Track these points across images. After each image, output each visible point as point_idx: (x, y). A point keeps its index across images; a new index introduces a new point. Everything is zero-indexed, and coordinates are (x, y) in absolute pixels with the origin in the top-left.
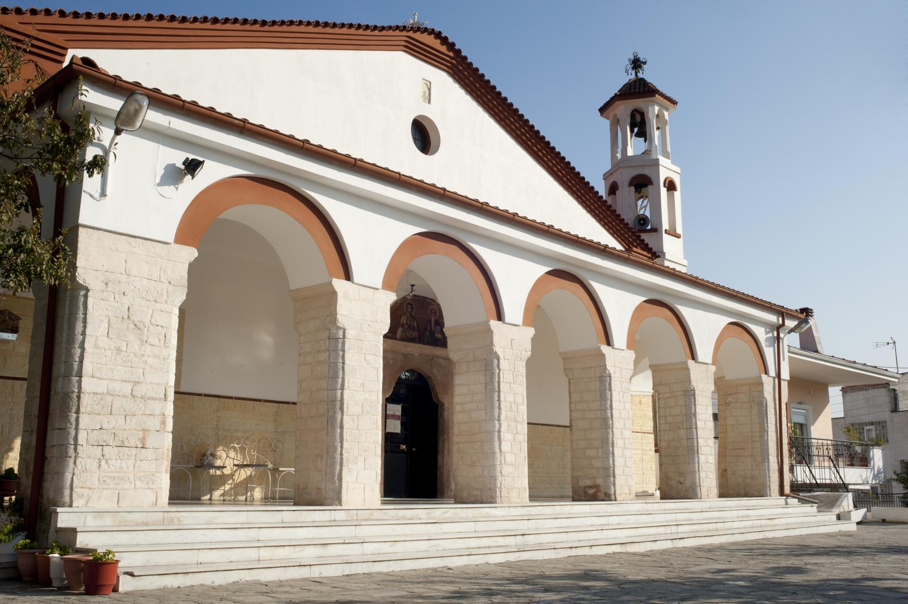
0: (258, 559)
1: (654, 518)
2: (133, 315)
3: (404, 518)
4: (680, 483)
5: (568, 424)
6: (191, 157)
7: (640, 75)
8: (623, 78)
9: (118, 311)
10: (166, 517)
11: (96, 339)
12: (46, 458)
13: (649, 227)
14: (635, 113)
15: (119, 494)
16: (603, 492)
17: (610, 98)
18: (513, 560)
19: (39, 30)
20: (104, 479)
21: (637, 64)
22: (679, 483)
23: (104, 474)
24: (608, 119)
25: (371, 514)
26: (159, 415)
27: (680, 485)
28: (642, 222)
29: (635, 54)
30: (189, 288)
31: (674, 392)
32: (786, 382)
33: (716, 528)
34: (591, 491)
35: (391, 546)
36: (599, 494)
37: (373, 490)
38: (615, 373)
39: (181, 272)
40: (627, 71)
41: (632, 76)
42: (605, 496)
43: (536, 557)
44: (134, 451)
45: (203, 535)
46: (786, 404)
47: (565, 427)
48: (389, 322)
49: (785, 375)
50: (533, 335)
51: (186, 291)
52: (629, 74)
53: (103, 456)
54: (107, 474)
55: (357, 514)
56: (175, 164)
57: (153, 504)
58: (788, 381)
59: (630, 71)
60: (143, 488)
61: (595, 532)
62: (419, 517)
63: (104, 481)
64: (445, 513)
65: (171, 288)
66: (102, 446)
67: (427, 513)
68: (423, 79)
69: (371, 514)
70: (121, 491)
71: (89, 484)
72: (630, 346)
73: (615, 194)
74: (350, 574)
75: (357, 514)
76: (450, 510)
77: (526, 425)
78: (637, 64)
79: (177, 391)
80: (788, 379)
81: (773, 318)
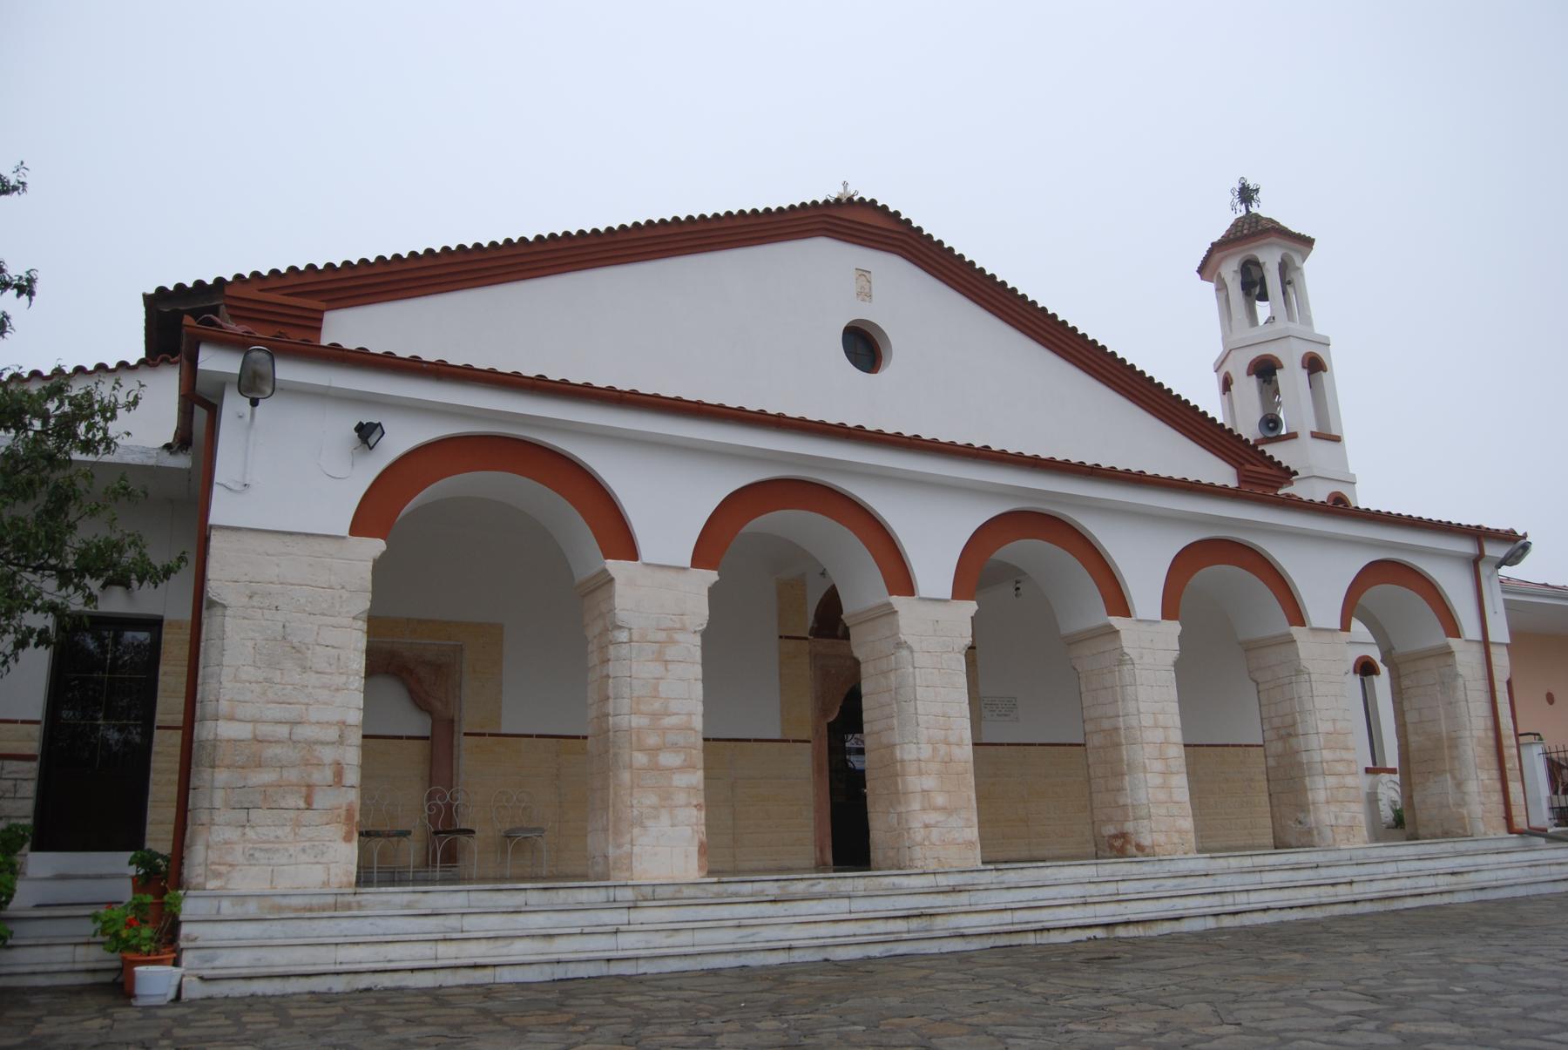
0: (434, 957)
1: (1215, 880)
2: (289, 635)
3: (736, 895)
4: (1300, 823)
5: (1262, 743)
6: (366, 419)
7: (1253, 209)
8: (1222, 217)
9: (269, 632)
10: (338, 900)
11: (237, 670)
12: (1504, 818)
13: (1284, 432)
14: (1249, 266)
15: (272, 871)
16: (1134, 843)
17: (1208, 251)
18: (878, 955)
19: (285, 295)
20: (251, 852)
21: (1246, 194)
22: (1297, 823)
23: (251, 845)
24: (1212, 281)
25: (679, 891)
26: (330, 765)
27: (1299, 826)
28: (1271, 425)
29: (1243, 181)
30: (373, 592)
31: (1279, 678)
32: (1504, 650)
33: (739, 956)
34: (1118, 843)
35: (667, 937)
36: (1129, 847)
37: (687, 856)
38: (1141, 658)
39: (363, 573)
40: (1234, 208)
41: (1241, 211)
42: (1137, 849)
43: (924, 949)
44: (292, 814)
45: (371, 924)
46: (1509, 683)
47: (1258, 746)
48: (707, 612)
49: (1499, 631)
50: (974, 612)
51: (369, 596)
52: (1238, 211)
53: (248, 821)
54: (256, 846)
55: (654, 892)
56: (1281, 367)
57: (324, 883)
58: (1507, 645)
59: (1238, 207)
60: (308, 863)
61: (1069, 908)
62: (766, 893)
63: (252, 855)
64: (813, 885)
65: (345, 595)
66: (248, 809)
67: (779, 887)
68: (857, 269)
69: (679, 891)
70: (276, 868)
71: (229, 859)
72: (1170, 609)
73: (1230, 390)
74: (565, 977)
75: (654, 892)
76: (822, 881)
77: (702, 741)
78: (1246, 194)
79: (366, 733)
80: (1508, 641)
81: (1467, 547)
